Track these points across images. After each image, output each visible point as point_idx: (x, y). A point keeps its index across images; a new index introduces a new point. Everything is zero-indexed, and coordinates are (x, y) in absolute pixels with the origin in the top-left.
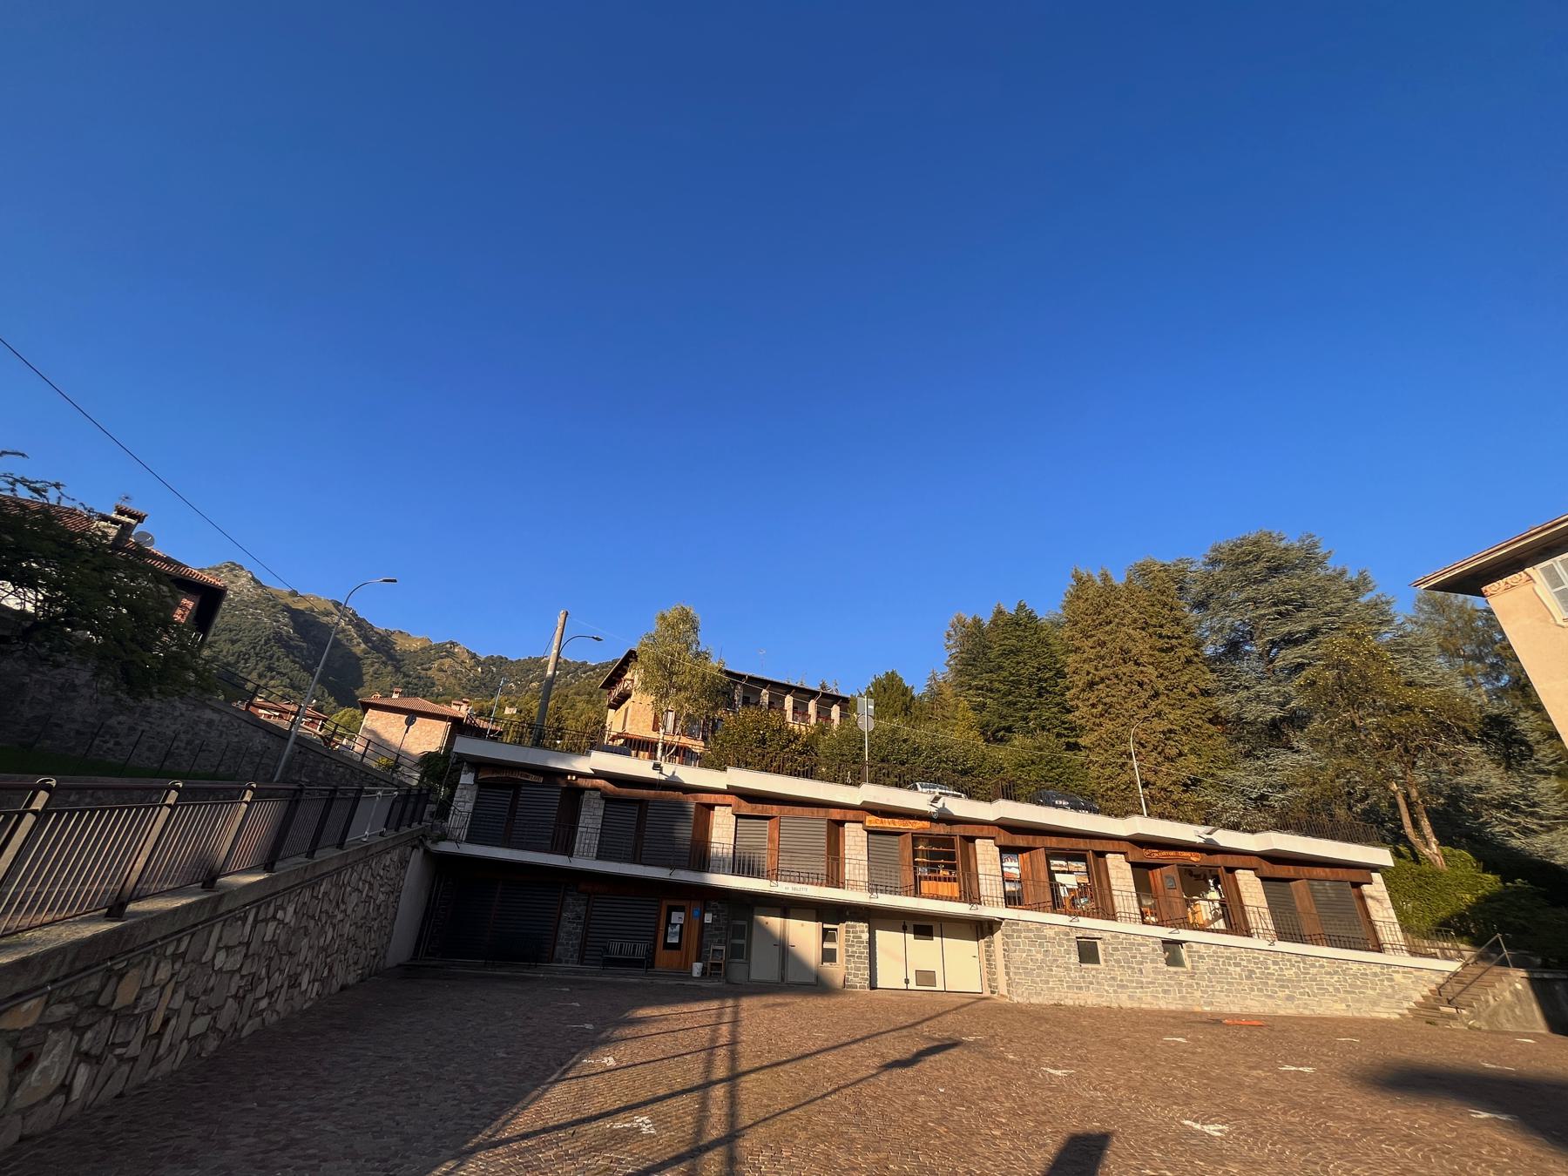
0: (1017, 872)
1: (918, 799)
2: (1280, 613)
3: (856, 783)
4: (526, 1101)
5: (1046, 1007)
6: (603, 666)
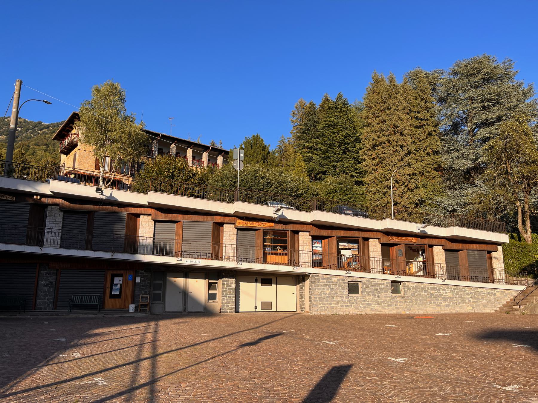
1: (267, 210)
2: (484, 107)
3: (231, 200)
4: (25, 375)
5: (329, 316)
6: (56, 126)
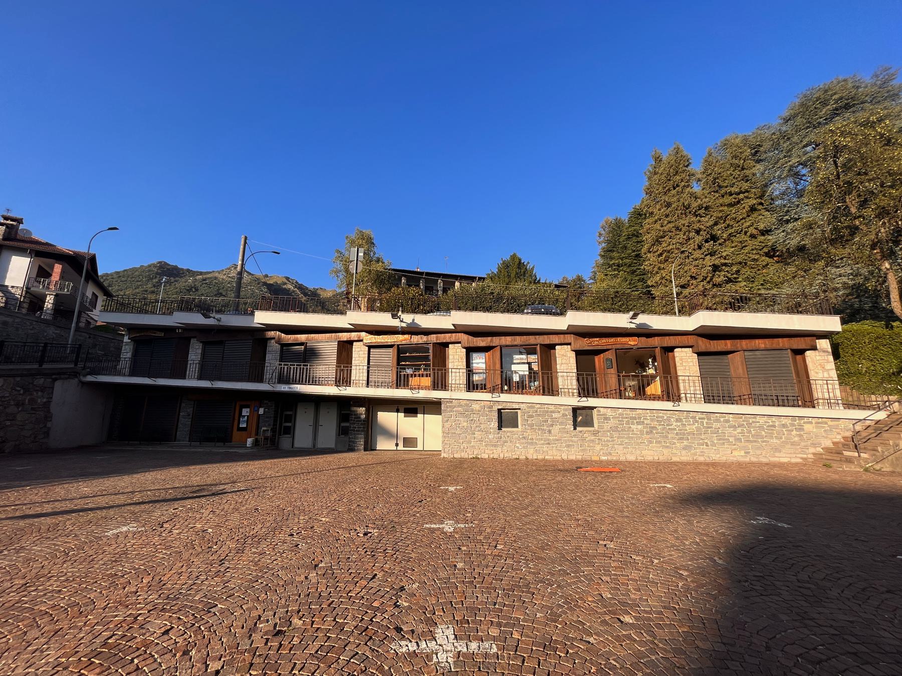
0: (484, 366)
